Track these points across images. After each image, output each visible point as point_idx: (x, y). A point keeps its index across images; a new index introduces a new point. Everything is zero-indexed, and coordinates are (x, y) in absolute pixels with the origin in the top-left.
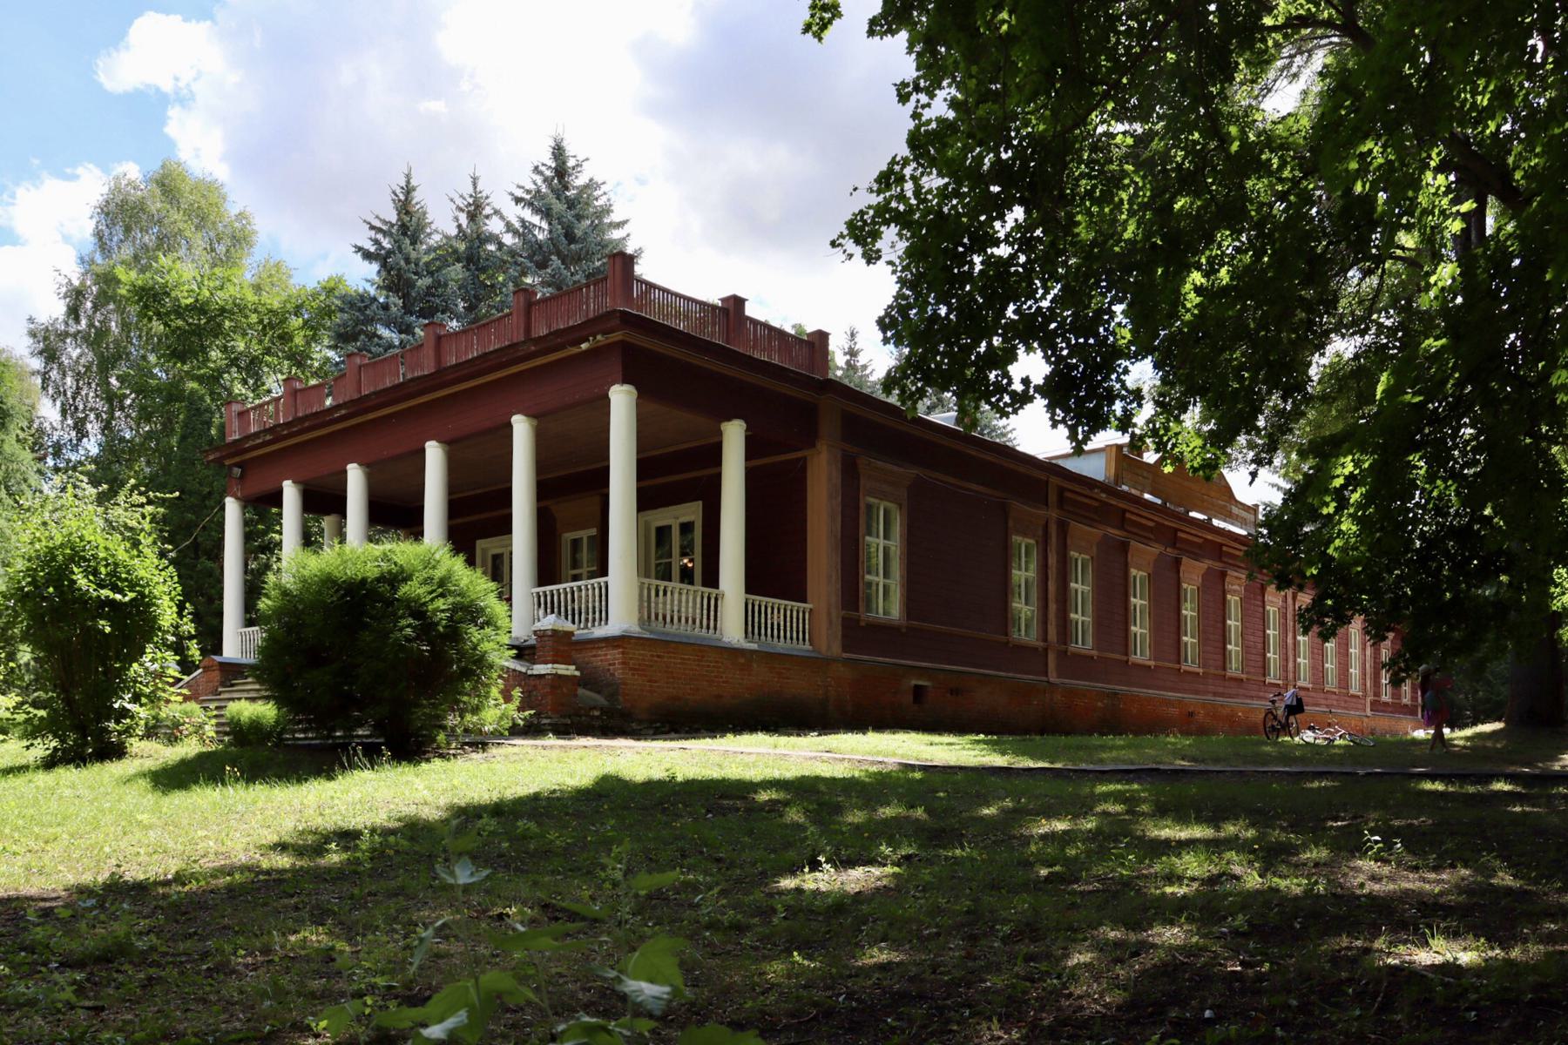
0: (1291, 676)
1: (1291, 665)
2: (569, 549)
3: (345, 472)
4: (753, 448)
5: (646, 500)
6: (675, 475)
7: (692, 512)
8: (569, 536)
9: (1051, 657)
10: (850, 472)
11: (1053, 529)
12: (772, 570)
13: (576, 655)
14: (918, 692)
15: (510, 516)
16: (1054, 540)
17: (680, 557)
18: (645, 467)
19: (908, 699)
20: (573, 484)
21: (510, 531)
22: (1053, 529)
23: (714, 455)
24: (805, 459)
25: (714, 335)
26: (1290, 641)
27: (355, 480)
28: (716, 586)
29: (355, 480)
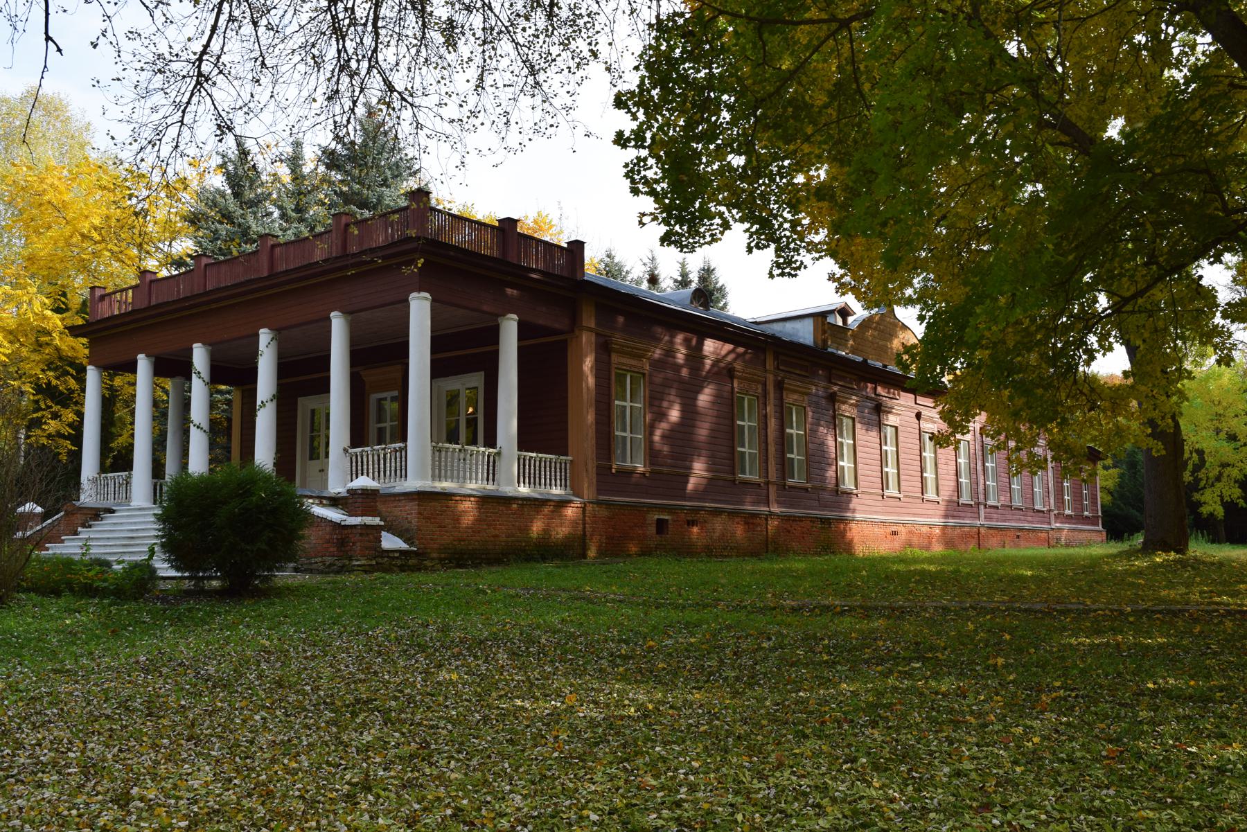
0: (981, 497)
1: (981, 487)
2: (376, 423)
3: (192, 349)
4: (524, 331)
5: (439, 369)
6: (462, 352)
7: (476, 380)
8: (374, 397)
9: (772, 489)
10: (604, 349)
11: (771, 388)
12: (542, 430)
13: (380, 506)
14: (661, 525)
15: (329, 378)
16: (772, 395)
17: (465, 426)
18: (438, 343)
19: (653, 530)
20: (380, 358)
21: (329, 392)
22: (771, 388)
23: (493, 336)
24: (565, 341)
25: (489, 248)
26: (979, 468)
27: (200, 357)
28: (493, 445)
29: (200, 357)
